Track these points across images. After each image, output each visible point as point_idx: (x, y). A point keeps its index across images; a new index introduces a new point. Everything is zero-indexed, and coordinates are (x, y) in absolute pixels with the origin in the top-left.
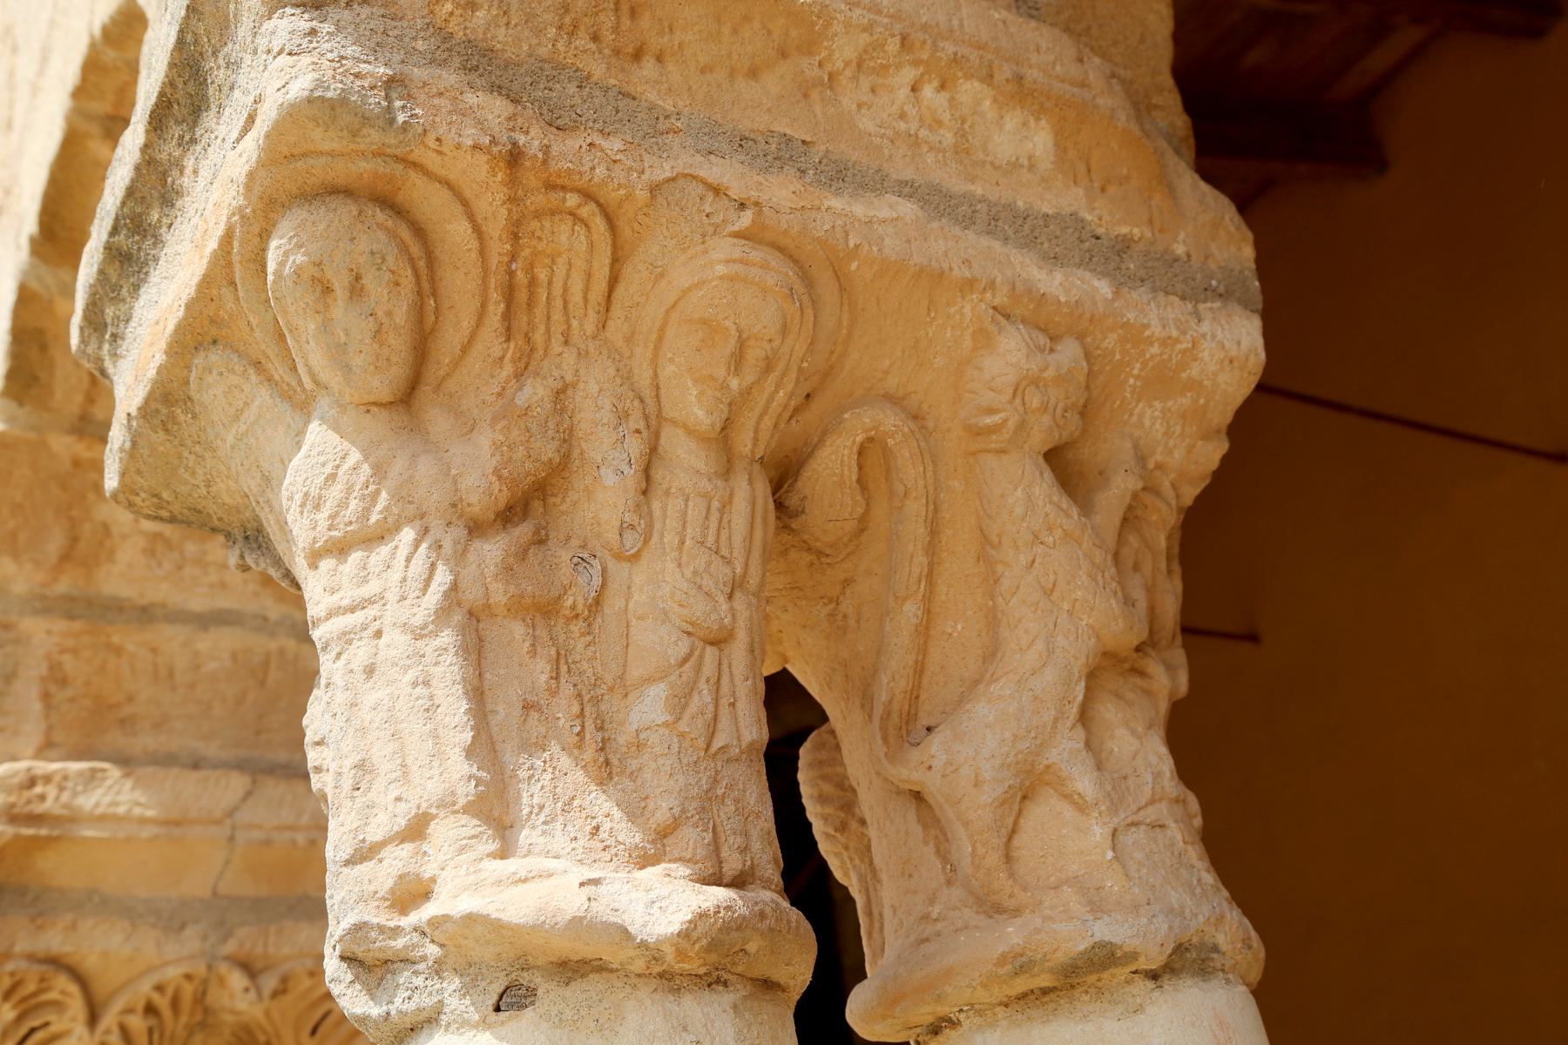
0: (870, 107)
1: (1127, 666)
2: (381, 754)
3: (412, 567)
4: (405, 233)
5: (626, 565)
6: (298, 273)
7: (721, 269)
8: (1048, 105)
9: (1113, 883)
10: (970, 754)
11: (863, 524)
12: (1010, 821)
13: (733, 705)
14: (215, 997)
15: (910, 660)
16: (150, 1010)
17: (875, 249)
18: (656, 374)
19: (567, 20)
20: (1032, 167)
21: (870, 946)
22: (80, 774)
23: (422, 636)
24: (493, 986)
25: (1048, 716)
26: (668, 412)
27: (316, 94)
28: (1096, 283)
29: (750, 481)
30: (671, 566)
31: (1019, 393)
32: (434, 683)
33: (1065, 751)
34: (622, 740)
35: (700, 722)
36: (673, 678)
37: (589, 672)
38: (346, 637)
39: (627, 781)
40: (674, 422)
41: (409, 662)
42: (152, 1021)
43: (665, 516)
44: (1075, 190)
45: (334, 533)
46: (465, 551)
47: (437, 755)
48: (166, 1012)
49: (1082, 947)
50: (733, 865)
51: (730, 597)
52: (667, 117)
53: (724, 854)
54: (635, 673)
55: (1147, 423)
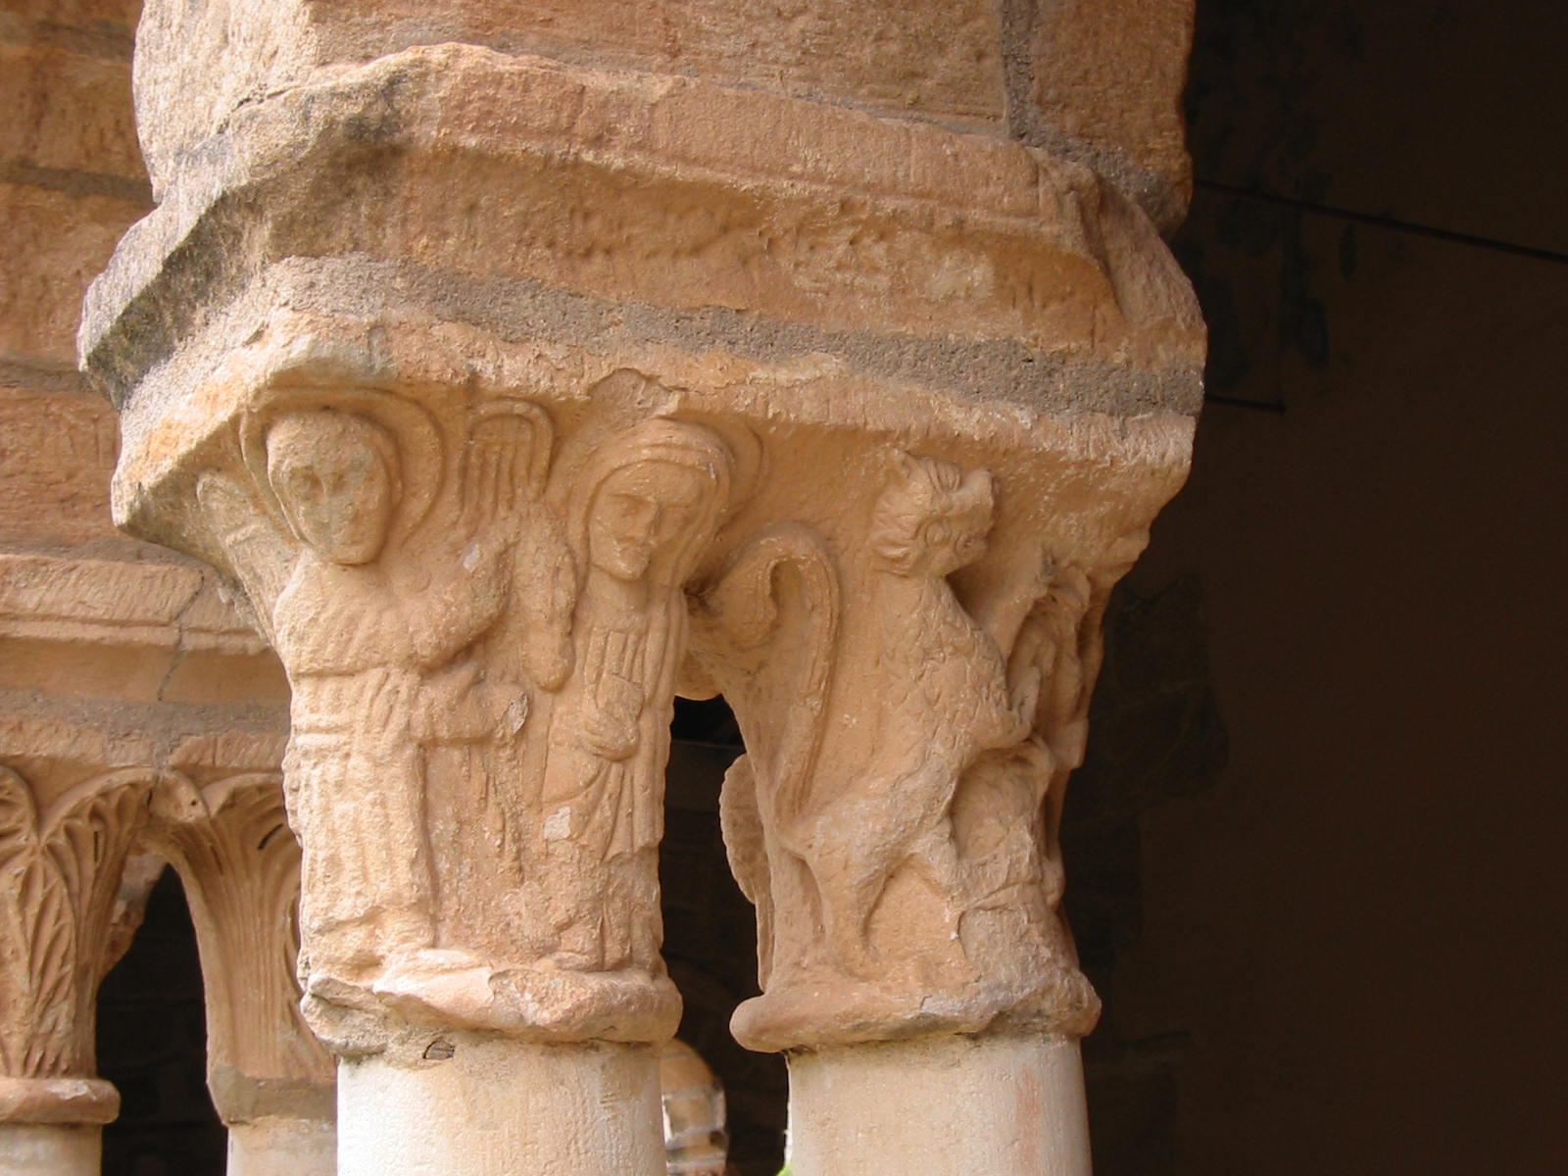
0: (807, 265)
1: (1010, 756)
2: (347, 853)
3: (375, 707)
4: (379, 439)
5: (549, 695)
6: (293, 474)
7: (646, 453)
8: (987, 242)
9: (952, 960)
10: (847, 831)
11: (776, 626)
12: (872, 899)
13: (631, 815)
14: (162, 808)
15: (807, 746)
16: (96, 815)
17: (792, 416)
18: (587, 529)
19: (527, 233)
20: (968, 297)
21: (763, 963)
22: (23, 565)
23: (381, 764)
24: (423, 1041)
25: (917, 812)
26: (598, 559)
27: (313, 356)
28: (1017, 413)
29: (667, 611)
30: (587, 697)
31: (922, 531)
32: (390, 804)
33: (931, 847)
34: (534, 849)
35: (599, 836)
36: (579, 799)
37: (513, 791)
38: (322, 754)
39: (536, 886)
40: (602, 570)
41: (370, 785)
42: (97, 827)
43: (586, 651)
44: (1011, 312)
45: (315, 665)
46: (417, 696)
47: (390, 863)
48: (112, 820)
49: (909, 1017)
50: (614, 952)
51: (638, 717)
52: (610, 311)
53: (608, 945)
54: (550, 790)
55: (1062, 531)
